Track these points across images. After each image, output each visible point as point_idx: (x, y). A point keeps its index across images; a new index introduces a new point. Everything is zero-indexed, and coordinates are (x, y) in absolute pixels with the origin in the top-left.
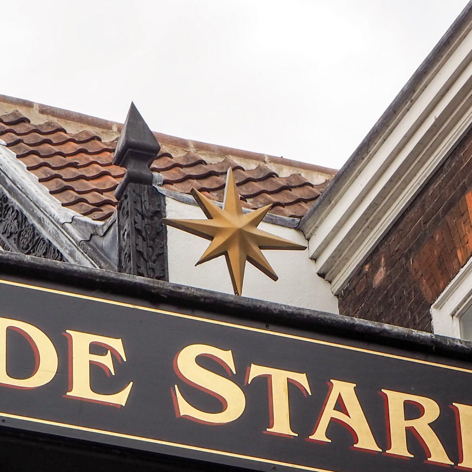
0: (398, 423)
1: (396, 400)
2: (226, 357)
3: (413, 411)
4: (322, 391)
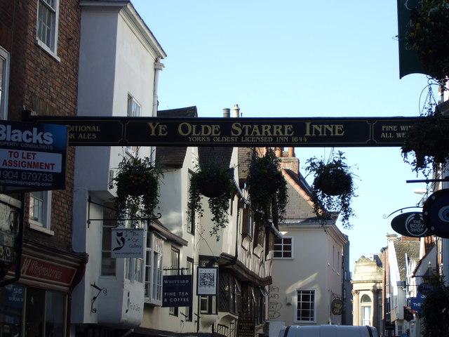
0: (264, 130)
1: (264, 126)
2: (239, 124)
3: (277, 128)
4: (253, 127)
